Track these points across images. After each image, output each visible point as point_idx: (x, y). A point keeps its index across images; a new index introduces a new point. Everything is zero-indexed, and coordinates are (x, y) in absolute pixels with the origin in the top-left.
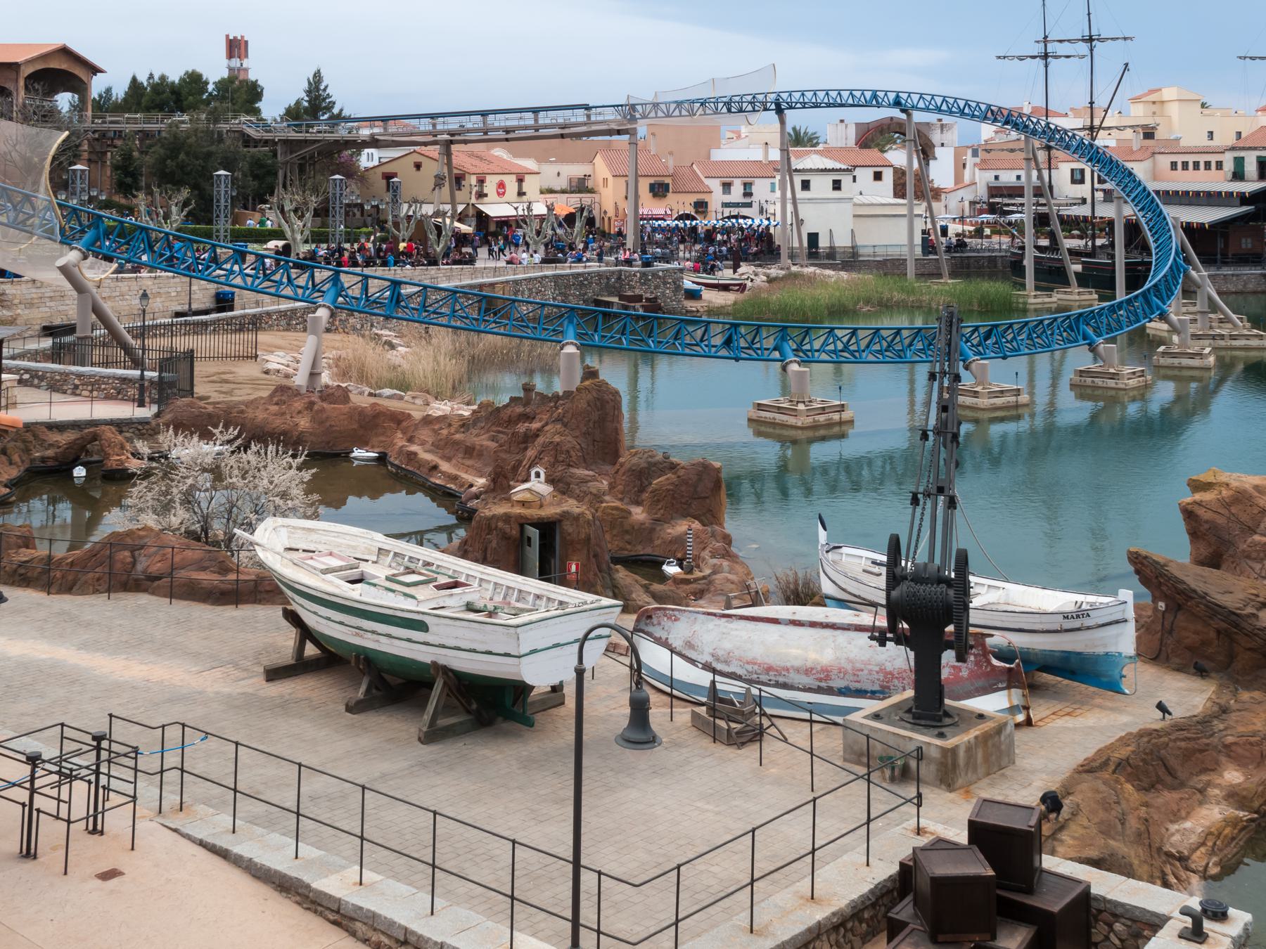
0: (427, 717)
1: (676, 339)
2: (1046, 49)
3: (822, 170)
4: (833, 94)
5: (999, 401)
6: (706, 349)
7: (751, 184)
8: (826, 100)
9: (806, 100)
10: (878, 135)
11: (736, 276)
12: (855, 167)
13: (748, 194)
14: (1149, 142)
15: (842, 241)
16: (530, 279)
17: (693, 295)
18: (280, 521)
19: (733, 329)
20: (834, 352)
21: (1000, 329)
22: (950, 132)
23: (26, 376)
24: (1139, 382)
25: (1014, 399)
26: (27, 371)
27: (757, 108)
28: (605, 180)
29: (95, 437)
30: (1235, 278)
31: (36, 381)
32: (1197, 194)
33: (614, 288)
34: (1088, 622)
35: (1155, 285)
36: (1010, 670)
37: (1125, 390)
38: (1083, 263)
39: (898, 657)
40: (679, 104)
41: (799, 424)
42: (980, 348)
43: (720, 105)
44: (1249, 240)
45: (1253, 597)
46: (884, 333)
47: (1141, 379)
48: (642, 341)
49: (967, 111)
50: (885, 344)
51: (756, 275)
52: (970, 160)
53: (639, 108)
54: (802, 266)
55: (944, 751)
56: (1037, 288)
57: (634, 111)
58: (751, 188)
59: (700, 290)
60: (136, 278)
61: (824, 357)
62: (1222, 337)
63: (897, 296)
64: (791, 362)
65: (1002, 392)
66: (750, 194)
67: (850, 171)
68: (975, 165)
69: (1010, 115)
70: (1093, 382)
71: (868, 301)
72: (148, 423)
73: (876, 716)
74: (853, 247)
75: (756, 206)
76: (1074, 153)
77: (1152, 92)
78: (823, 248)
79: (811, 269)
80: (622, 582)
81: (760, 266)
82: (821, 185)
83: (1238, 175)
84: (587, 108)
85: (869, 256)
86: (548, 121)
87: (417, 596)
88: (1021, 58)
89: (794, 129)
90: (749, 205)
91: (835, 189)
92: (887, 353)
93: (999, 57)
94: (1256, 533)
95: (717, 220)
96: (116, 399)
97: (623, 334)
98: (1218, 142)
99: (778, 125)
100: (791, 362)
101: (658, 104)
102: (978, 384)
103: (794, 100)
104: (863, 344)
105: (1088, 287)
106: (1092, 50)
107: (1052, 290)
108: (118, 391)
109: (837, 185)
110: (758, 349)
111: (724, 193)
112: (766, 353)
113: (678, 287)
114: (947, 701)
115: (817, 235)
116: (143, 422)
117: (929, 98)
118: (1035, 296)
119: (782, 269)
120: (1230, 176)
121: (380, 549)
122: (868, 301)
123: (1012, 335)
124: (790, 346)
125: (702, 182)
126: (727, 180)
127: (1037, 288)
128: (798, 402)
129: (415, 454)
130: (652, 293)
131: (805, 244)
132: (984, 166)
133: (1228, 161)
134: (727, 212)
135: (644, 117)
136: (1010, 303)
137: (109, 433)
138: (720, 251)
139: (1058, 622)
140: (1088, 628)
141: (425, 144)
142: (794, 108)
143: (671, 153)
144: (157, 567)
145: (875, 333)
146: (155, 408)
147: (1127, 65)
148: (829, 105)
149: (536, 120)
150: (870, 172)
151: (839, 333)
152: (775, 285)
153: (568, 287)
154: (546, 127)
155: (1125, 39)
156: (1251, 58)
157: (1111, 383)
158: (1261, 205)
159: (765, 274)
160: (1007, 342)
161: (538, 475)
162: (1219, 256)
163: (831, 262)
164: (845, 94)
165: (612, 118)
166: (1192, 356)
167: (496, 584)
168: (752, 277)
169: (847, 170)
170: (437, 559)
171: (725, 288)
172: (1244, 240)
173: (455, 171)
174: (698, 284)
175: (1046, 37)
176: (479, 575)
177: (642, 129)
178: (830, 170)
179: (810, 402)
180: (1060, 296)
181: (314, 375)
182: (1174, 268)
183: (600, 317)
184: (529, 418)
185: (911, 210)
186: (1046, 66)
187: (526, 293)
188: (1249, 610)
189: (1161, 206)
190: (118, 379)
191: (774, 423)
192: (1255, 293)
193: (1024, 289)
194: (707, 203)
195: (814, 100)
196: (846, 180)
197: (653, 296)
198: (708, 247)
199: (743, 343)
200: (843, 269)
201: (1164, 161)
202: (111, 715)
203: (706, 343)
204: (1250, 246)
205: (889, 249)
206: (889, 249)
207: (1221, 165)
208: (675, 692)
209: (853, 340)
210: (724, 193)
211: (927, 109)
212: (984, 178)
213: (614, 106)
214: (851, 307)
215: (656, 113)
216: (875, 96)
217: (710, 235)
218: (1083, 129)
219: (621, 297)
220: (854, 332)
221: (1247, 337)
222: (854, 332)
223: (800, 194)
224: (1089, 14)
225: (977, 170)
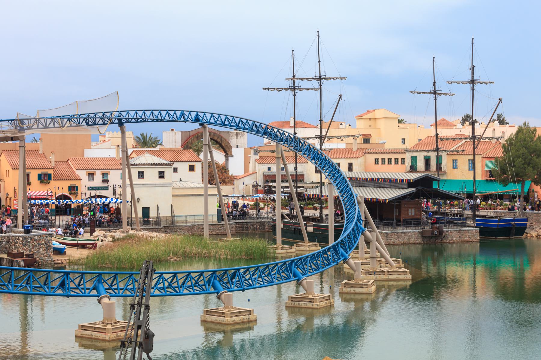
1: (27, 283)
2: (294, 84)
3: (152, 165)
5: (237, 319)
7: (107, 174)
8: (151, 117)
9: (138, 117)
10: (195, 139)
11: (92, 238)
13: (105, 181)
14: (367, 145)
15: (165, 213)
17: (59, 252)
19: (65, 276)
20: (163, 288)
22: (242, 138)
24: (326, 303)
25: (247, 317)
27: (106, 122)
28: (8, 172)
30: (403, 235)
32: (384, 180)
33: (5, 248)
35: (342, 241)
37: (317, 309)
38: (314, 226)
40: (53, 119)
41: (107, 338)
42: (250, 281)
43: (81, 120)
44: (413, 210)
46: (194, 275)
47: (327, 301)
49: (227, 123)
50: (194, 282)
51: (105, 237)
52: (253, 158)
53: (26, 121)
54: (137, 230)
56: (284, 243)
57: (23, 124)
58: (107, 177)
59: (65, 249)
61: (157, 292)
63: (195, 250)
64: (104, 297)
65: (240, 312)
66: (107, 181)
67: (170, 165)
68: (256, 160)
69: (266, 128)
70: (299, 304)
71: (175, 254)
74: (172, 217)
75: (111, 189)
76: (304, 154)
77: (369, 112)
78: (153, 218)
79: (145, 232)
81: (109, 230)
82: (151, 175)
83: (413, 168)
85: (183, 222)
88: (279, 90)
90: (106, 188)
91: (160, 177)
93: (265, 89)
95: (82, 199)
98: (408, 145)
99: (120, 134)
100: (104, 297)
101: (39, 119)
102: (225, 308)
103: (130, 117)
104: (181, 282)
105: (315, 241)
106: (321, 85)
107: (292, 244)
109: (161, 175)
110: (82, 289)
111: (89, 180)
112: (87, 291)
113: (48, 247)
115: (148, 209)
117: (217, 116)
118: (282, 249)
119: (123, 232)
120: (408, 169)
122: (175, 254)
123: (249, 275)
124: (102, 287)
125: (74, 173)
127: (284, 243)
128: (108, 324)
130: (30, 251)
131: (140, 214)
132: (262, 160)
133: (408, 157)
134: (93, 193)
135: (29, 128)
136: (265, 253)
138: (84, 221)
142: (131, 122)
143: (53, 153)
147: (341, 96)
148: (153, 121)
150: (186, 165)
151: (166, 276)
152: (116, 244)
155: (341, 78)
156: (418, 93)
157: (309, 305)
158: (420, 188)
159: (111, 236)
160: (246, 280)
162: (395, 221)
163: (157, 227)
164: (148, 113)
165: (7, 128)
166: (362, 286)
168: (103, 238)
169: (168, 164)
171: (83, 246)
172: (410, 210)
174: (63, 244)
175: (294, 77)
177: (28, 135)
178: (157, 165)
179: (115, 323)
180: (298, 248)
182: (355, 229)
185: (206, 191)
186: (294, 96)
189: (352, 188)
191: (91, 338)
192: (415, 244)
193: (275, 243)
194: (77, 187)
195: (143, 117)
196: (168, 172)
197: (32, 253)
198: (75, 218)
199: (72, 285)
200: (165, 232)
201: (371, 158)
203: (82, 286)
204: (413, 214)
205: (196, 218)
206: (196, 218)
207: (404, 161)
209: (175, 280)
210: (89, 180)
211: (216, 124)
212: (262, 169)
213: (8, 120)
214: (164, 258)
215: (38, 126)
216: (183, 115)
217: (79, 210)
218: (315, 138)
219: (9, 254)
220: (175, 275)
222: (175, 275)
223: (136, 180)
224: (319, 62)
225: (257, 164)
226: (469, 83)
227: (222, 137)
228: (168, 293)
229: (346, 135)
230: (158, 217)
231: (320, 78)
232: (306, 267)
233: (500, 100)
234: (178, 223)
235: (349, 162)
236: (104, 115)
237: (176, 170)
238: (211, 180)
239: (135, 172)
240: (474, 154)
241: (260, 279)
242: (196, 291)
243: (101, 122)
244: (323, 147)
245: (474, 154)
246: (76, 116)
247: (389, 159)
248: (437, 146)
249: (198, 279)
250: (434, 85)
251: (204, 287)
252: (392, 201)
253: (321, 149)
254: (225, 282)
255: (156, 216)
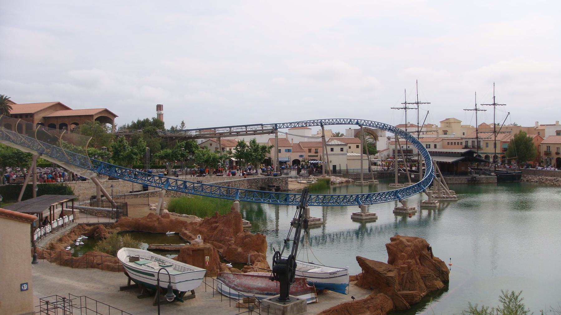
0: (155, 299)
3: (337, 145)
4: (338, 120)
6: (295, 202)
8: (336, 122)
9: (330, 122)
12: (348, 143)
15: (343, 168)
16: (240, 180)
18: (126, 248)
19: (287, 196)
20: (333, 203)
21: (371, 195)
23: (83, 210)
26: (83, 209)
29: (98, 228)
31: (86, 212)
34: (336, 275)
36: (312, 288)
38: (414, 175)
39: (275, 284)
44: (464, 167)
45: (387, 269)
48: (276, 201)
50: (348, 200)
55: (284, 307)
60: (118, 181)
62: (444, 197)
69: (390, 127)
72: (113, 224)
73: (270, 300)
74: (347, 170)
75: (319, 156)
80: (222, 267)
82: (337, 150)
84: (262, 125)
85: (352, 172)
86: (250, 130)
87: (154, 268)
88: (398, 109)
89: (441, 122)
90: (317, 156)
91: (341, 151)
92: (348, 203)
93: (392, 108)
94: (403, 252)
96: (107, 217)
97: (270, 199)
106: (418, 107)
108: (107, 215)
114: (290, 295)
116: (113, 224)
117: (367, 122)
121: (152, 256)
123: (384, 196)
126: (310, 148)
129: (186, 233)
133: (464, 141)
135: (280, 128)
137: (102, 227)
139: (328, 276)
140: (336, 277)
141: (212, 138)
142: (326, 125)
144: (99, 262)
145: (332, 197)
146: (116, 220)
147: (428, 111)
148: (337, 124)
149: (246, 129)
153: (252, 183)
154: (249, 131)
155: (428, 103)
157: (404, 212)
160: (383, 198)
161: (199, 237)
164: (334, 120)
167: (179, 266)
170: (166, 259)
172: (462, 167)
173: (222, 146)
175: (406, 102)
176: (175, 263)
181: (161, 210)
183: (263, 193)
184: (216, 222)
186: (406, 111)
187: (238, 185)
188: (384, 272)
190: (107, 211)
195: (332, 122)
196: (345, 148)
197: (279, 185)
202: (69, 294)
203: (295, 201)
208: (231, 297)
209: (339, 199)
211: (366, 125)
220: (325, 196)
221: (451, 198)
222: (325, 196)
223: (329, 152)
224: (417, 95)
226: (493, 105)
227: (373, 132)
228: (335, 205)
229: (473, 137)
230: (340, 170)
231: (418, 103)
232: (404, 194)
233: (509, 113)
234: (350, 172)
235: (435, 144)
236: (314, 121)
237: (350, 147)
238: (364, 152)
239: (329, 148)
240: (495, 140)
241: (381, 199)
242: (321, 204)
243: (313, 125)
244: (419, 137)
245: (495, 140)
246: (301, 122)
247: (454, 142)
248: (477, 136)
249: (350, 199)
250: (476, 106)
251: (353, 202)
252: (453, 163)
253: (418, 138)
254: (374, 199)
255: (339, 169)
